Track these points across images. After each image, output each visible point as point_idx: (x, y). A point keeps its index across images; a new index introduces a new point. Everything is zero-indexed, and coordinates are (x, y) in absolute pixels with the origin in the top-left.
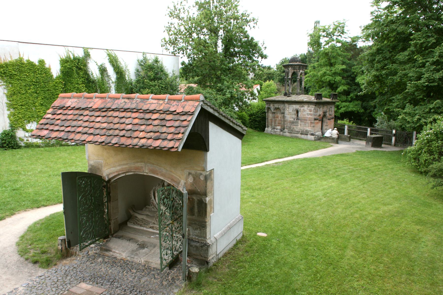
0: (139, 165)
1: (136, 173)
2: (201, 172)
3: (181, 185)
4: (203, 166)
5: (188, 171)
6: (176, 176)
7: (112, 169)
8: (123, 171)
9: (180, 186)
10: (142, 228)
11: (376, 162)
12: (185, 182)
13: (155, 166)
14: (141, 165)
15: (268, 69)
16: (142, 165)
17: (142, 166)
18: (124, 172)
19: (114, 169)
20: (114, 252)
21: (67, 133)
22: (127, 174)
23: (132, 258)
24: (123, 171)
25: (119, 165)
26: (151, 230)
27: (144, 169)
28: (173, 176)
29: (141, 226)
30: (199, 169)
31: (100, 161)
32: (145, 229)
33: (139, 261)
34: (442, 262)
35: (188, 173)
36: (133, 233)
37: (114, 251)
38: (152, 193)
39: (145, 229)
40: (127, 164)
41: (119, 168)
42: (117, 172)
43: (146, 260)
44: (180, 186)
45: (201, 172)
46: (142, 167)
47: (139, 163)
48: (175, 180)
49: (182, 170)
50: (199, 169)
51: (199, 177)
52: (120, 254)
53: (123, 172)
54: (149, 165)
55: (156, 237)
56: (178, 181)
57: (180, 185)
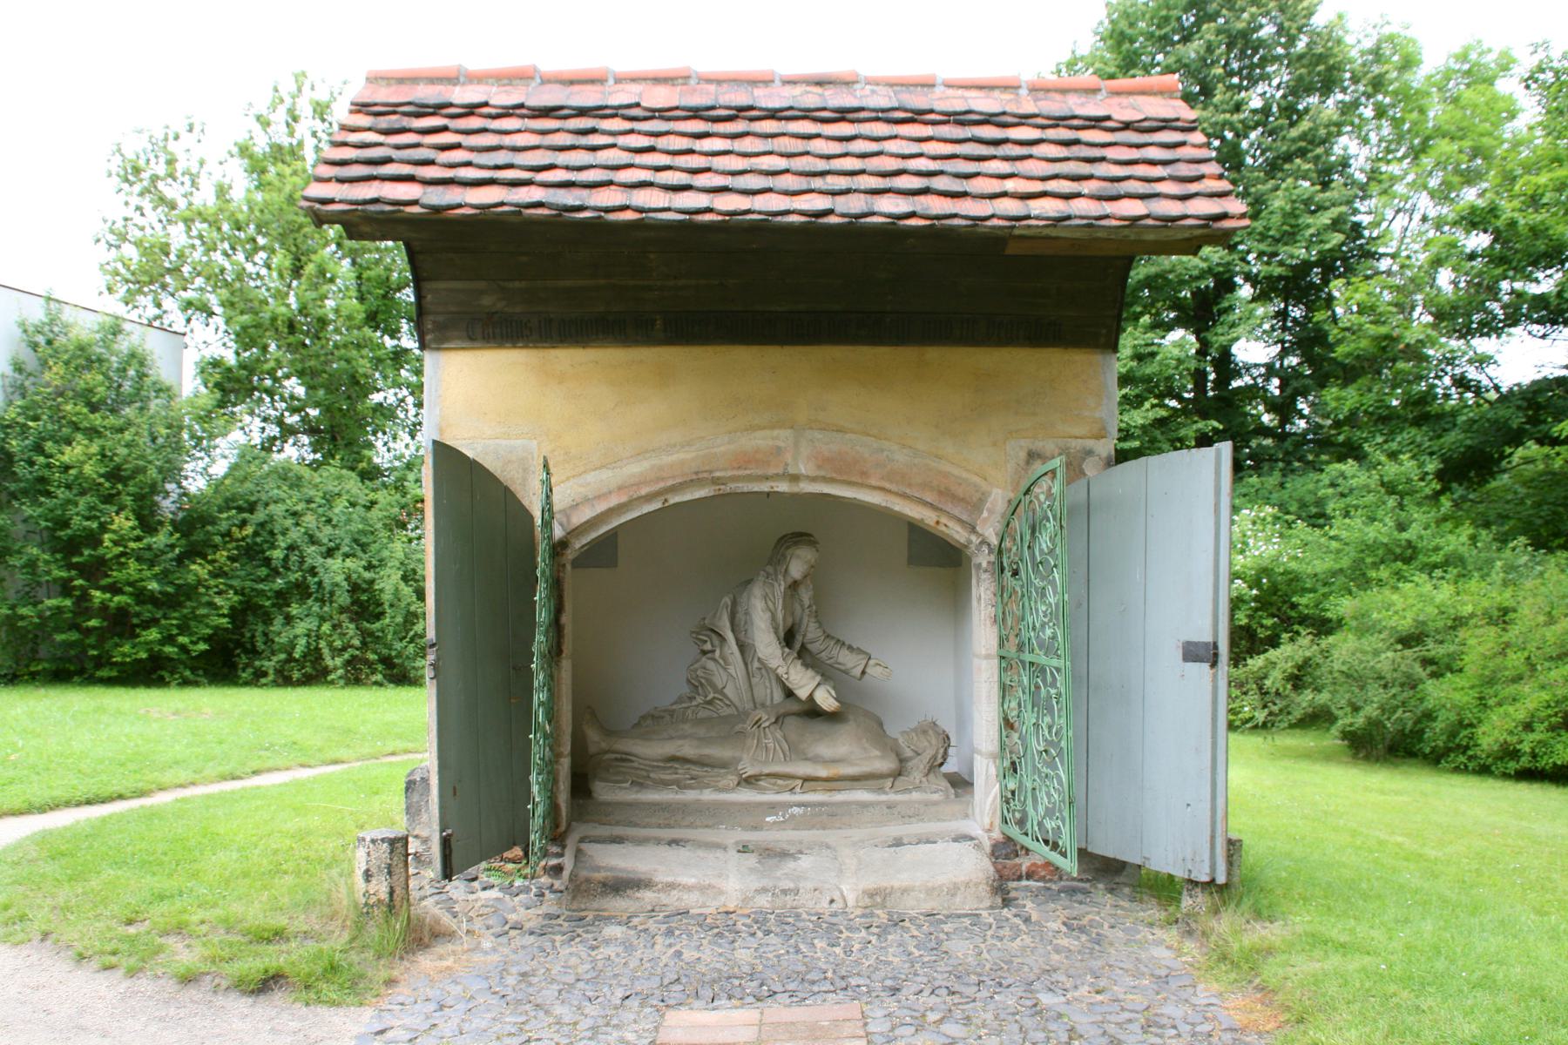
0: (761, 440)
1: (727, 489)
2: (1090, 443)
3: (991, 512)
4: (1097, 415)
5: (1023, 443)
6: (965, 475)
7: (591, 477)
8: (663, 479)
9: (985, 520)
10: (690, 795)
11: (745, 828)
12: (1012, 495)
13: (853, 436)
14: (771, 443)
15: (1131, 60)
16: (783, 437)
17: (782, 444)
18: (670, 483)
19: (605, 475)
20: (672, 886)
21: (868, 196)
22: (675, 499)
23: (784, 892)
24: (663, 479)
25: (641, 454)
26: (746, 795)
27: (789, 457)
28: (946, 475)
29: (682, 786)
30: (1077, 431)
31: (519, 442)
32: (708, 796)
33: (825, 904)
34: (1564, 1026)
35: (1023, 455)
36: (654, 820)
37: (670, 879)
38: (728, 624)
39: (708, 796)
40: (689, 444)
41: (635, 469)
42: (620, 488)
43: (870, 883)
44: (985, 520)
45: (1090, 443)
46: (778, 451)
47: (759, 434)
48: (960, 492)
49: (994, 444)
50: (1077, 431)
51: (1080, 466)
52: (703, 889)
53: (662, 485)
54: (818, 435)
55: (793, 816)
56: (978, 495)
57: (985, 514)
